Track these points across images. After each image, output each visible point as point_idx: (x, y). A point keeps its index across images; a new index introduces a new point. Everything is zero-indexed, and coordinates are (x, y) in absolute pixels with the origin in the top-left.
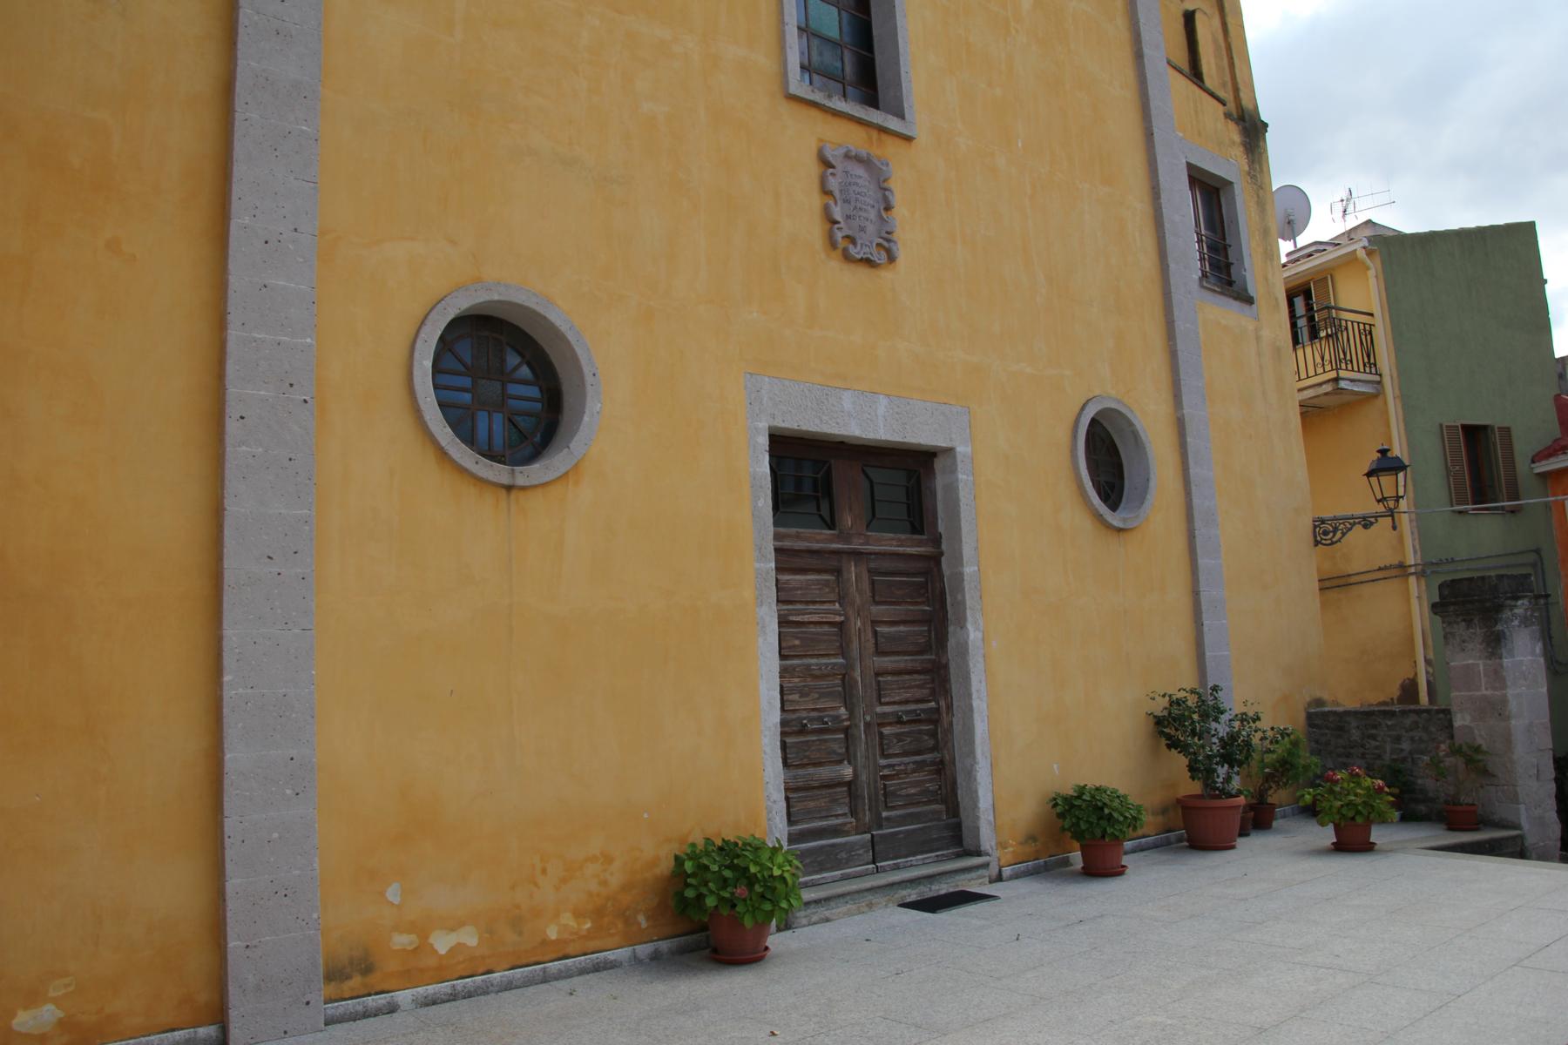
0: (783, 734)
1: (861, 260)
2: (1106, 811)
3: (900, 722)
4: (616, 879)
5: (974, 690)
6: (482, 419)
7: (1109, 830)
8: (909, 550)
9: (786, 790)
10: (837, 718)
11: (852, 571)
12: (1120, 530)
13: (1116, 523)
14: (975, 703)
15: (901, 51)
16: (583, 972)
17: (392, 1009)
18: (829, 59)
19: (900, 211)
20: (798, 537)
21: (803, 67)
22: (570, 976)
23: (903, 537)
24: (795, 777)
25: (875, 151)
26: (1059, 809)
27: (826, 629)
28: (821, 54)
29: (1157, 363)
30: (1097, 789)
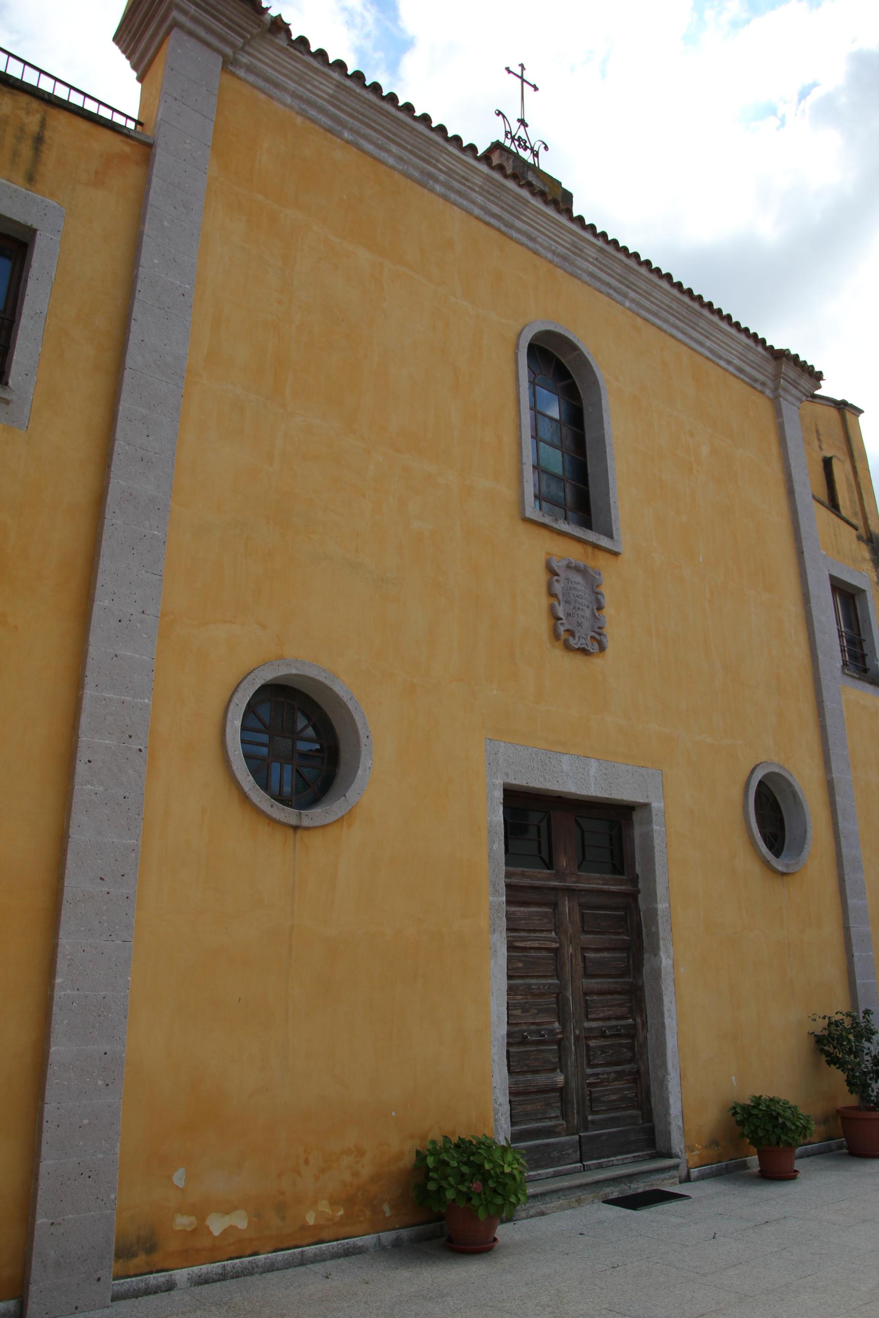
0: (509, 1044)
1: (579, 649)
2: (780, 1120)
3: (603, 1036)
4: (366, 1171)
5: (665, 1009)
6: (276, 767)
7: (784, 1138)
8: (613, 888)
9: (511, 1093)
10: (551, 1032)
11: (566, 905)
12: (783, 874)
13: (781, 868)
14: (667, 1021)
15: (611, 486)
16: (335, 1256)
17: (170, 1286)
18: (554, 490)
19: (609, 611)
20: (523, 875)
21: (536, 496)
22: (324, 1260)
23: (607, 876)
24: (516, 1083)
25: (590, 563)
26: (739, 1117)
27: (544, 954)
28: (548, 486)
29: (811, 735)
30: (771, 1100)
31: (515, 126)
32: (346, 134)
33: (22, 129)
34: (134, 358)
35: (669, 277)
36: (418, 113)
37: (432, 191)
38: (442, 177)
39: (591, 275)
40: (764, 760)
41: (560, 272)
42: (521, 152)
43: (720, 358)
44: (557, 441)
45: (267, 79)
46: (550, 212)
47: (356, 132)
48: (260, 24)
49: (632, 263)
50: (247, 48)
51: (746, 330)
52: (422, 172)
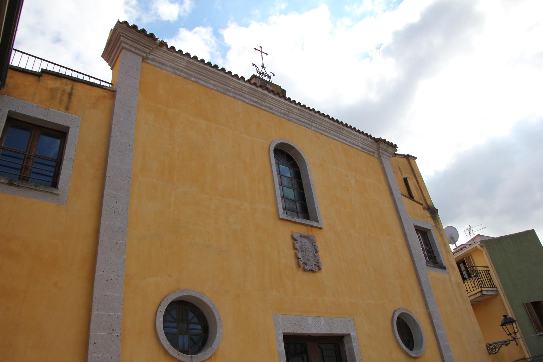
6: (180, 337)
12: (415, 358)
13: (413, 355)
18: (292, 206)
19: (321, 252)
21: (283, 209)
28: (289, 204)
31: (260, 69)
32: (193, 79)
33: (64, 91)
34: (110, 172)
35: (328, 116)
36: (220, 68)
37: (229, 95)
38: (232, 90)
39: (297, 119)
40: (398, 307)
41: (284, 120)
42: (264, 78)
43: (354, 144)
44: (291, 186)
45: (160, 63)
46: (277, 97)
47: (197, 78)
48: (155, 44)
49: (312, 113)
50: (151, 53)
51: (363, 132)
52: (224, 89)
